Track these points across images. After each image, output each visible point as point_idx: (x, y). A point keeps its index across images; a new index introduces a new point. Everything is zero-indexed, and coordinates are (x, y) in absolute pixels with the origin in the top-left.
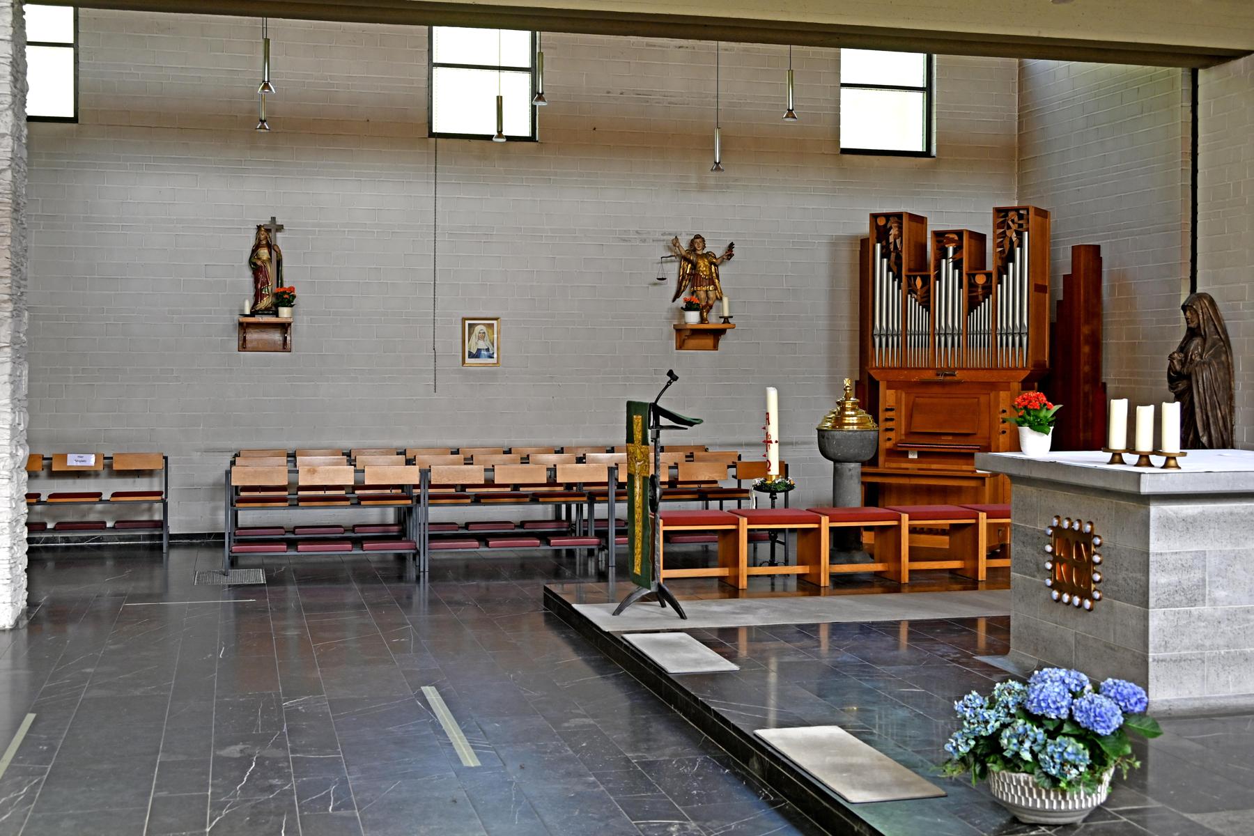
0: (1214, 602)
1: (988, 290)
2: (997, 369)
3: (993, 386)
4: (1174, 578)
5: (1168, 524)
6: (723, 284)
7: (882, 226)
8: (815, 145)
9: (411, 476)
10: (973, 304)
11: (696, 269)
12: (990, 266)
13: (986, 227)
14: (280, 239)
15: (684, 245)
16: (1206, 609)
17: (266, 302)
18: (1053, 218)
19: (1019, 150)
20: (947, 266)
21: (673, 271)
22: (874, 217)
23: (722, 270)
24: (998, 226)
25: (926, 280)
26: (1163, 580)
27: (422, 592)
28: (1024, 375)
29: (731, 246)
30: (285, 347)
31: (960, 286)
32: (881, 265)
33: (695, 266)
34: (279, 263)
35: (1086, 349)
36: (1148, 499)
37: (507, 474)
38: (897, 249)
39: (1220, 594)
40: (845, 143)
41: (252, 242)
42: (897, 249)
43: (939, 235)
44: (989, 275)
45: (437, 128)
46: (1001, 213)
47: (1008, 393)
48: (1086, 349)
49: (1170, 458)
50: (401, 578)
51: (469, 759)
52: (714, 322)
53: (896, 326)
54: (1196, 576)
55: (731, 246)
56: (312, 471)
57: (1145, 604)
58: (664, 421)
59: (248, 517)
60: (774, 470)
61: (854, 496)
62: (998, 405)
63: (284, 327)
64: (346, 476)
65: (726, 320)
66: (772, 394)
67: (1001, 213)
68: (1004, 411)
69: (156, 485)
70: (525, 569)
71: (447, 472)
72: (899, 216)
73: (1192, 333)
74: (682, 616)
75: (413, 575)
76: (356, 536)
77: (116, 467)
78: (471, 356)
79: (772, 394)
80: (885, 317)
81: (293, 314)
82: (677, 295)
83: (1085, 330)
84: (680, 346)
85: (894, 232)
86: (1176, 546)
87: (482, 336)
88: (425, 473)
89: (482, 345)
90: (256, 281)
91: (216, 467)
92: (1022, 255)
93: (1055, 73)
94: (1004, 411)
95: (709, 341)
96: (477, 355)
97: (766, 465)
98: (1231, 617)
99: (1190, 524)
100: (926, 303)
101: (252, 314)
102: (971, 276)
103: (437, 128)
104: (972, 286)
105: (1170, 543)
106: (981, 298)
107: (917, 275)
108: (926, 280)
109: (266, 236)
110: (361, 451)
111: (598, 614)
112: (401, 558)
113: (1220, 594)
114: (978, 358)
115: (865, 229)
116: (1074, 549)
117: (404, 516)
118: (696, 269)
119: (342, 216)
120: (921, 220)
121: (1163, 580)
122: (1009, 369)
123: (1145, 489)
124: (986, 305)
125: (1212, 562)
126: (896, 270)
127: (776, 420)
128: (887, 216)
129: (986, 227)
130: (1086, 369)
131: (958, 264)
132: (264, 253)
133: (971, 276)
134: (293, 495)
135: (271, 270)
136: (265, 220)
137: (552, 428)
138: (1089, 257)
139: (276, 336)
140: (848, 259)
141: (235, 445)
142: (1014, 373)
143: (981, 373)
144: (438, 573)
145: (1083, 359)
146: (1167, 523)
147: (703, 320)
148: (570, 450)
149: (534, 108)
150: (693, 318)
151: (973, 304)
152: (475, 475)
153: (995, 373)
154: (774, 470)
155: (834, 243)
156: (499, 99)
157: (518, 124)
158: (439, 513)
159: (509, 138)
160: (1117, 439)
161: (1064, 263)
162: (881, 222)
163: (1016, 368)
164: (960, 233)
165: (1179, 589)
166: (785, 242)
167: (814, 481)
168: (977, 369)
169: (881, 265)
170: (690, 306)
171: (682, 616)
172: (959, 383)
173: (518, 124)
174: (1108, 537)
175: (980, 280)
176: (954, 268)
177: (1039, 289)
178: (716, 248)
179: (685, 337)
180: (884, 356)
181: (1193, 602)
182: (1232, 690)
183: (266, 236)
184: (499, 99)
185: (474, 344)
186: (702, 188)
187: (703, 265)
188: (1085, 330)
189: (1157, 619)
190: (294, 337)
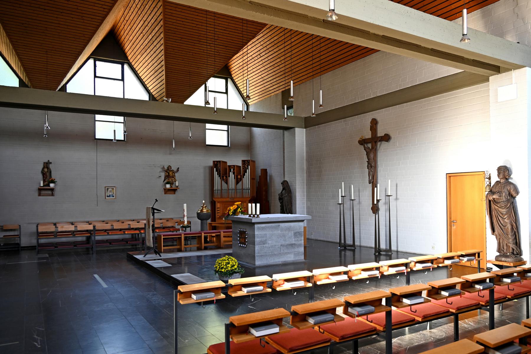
0: (269, 244)
1: (241, 179)
4: (260, 239)
5: (259, 228)
6: (176, 178)
7: (216, 164)
8: (200, 144)
9: (91, 227)
11: (169, 174)
12: (242, 174)
13: (240, 164)
14: (51, 166)
15: (166, 168)
16: (267, 245)
17: (46, 183)
18: (256, 163)
19: (249, 146)
20: (231, 174)
21: (163, 175)
22: (214, 162)
23: (176, 174)
24: (243, 164)
25: (226, 177)
26: (258, 240)
27: (95, 255)
28: (249, 199)
29: (178, 168)
30: (53, 195)
32: (215, 173)
33: (169, 173)
34: (50, 172)
35: (264, 193)
36: (254, 224)
37: (117, 226)
38: (220, 169)
39: (270, 242)
40: (207, 143)
41: (42, 167)
42: (220, 169)
43: (229, 166)
45: (97, 137)
46: (243, 161)
48: (264, 193)
49: (258, 215)
50: (88, 254)
51: (105, 286)
52: (174, 187)
53: (219, 188)
54: (265, 239)
55: (178, 168)
56: (62, 227)
57: (254, 245)
58: (155, 211)
59: (42, 241)
60: (186, 223)
61: (207, 228)
63: (52, 190)
64: (72, 228)
65: (177, 187)
66: (185, 205)
67: (243, 161)
69: (16, 233)
70: (123, 250)
71: (99, 226)
72: (220, 162)
73: (283, 189)
74: (161, 256)
75: (91, 252)
76: (75, 244)
77: (4, 228)
78: (108, 196)
79: (185, 205)
80: (217, 186)
81: (55, 185)
82: (164, 181)
83: (264, 188)
84: (165, 194)
85: (219, 165)
86: (260, 233)
87: (111, 191)
88: (94, 227)
89: (111, 194)
90: (44, 177)
91: (33, 228)
92: (248, 171)
93: (256, 130)
95: (173, 192)
96: (109, 196)
97: (184, 222)
98: (272, 247)
99: (263, 228)
100: (227, 182)
101: (44, 186)
102: (237, 176)
103: (97, 137)
105: (259, 232)
107: (224, 177)
108: (226, 177)
109: (47, 165)
110: (76, 222)
111: (140, 257)
112: (87, 249)
113: (270, 242)
115: (211, 164)
116: (242, 234)
117: (88, 238)
118: (169, 174)
119: (69, 161)
120: (226, 163)
121: (258, 240)
123: (253, 221)
124: (240, 183)
125: (268, 236)
126: (219, 174)
127: (187, 211)
128: (217, 162)
129: (240, 164)
131: (234, 173)
132: (46, 170)
133: (237, 176)
134: (55, 234)
135: (48, 174)
136: (46, 161)
137: (126, 214)
138: (265, 171)
139: (50, 192)
140: (208, 171)
141: (38, 222)
144: (98, 252)
146: (259, 228)
147: (171, 187)
148: (136, 220)
149: (124, 135)
150: (168, 186)
151: (237, 182)
152: (108, 227)
154: (186, 223)
155: (205, 168)
156: (115, 131)
157: (120, 136)
158: (98, 238)
159: (117, 140)
160: (250, 213)
161: (259, 173)
162: (216, 163)
164: (234, 166)
165: (261, 241)
166: (192, 167)
167: (196, 226)
169: (215, 173)
170: (168, 183)
171: (161, 256)
173: (120, 136)
174: (248, 231)
175: (239, 177)
177: (252, 179)
178: (174, 168)
179: (167, 191)
180: (217, 194)
181: (264, 244)
182: (272, 261)
183: (47, 165)
184: (115, 131)
185: (108, 194)
186: (170, 154)
187: (171, 173)
188: (264, 188)
189: (257, 248)
190: (56, 193)
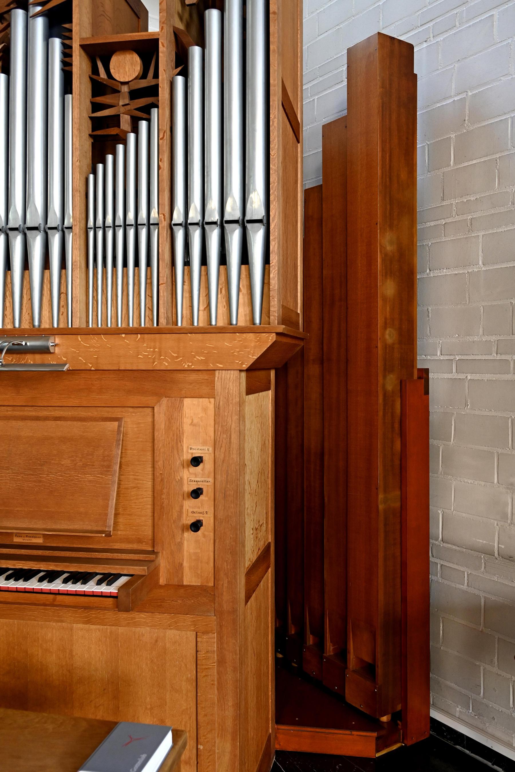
1: (146, 97)
2: (174, 330)
3: (158, 383)
10: (103, 140)
20: (220, 391)
28: (255, 347)
31: (67, 87)
44: (147, 50)
47: (209, 404)
48: (388, 288)
62: (178, 439)
68: (196, 461)
94: (196, 461)
104: (100, 88)
106: (125, 122)
114: (121, 299)
122: (209, 330)
124: (137, 147)
130: (389, 336)
142: (226, 342)
143: (128, 340)
145: (383, 311)
151: (103, 140)
153: (169, 341)
161: (324, 98)
163: (230, 329)
168: (116, 332)
172: (57, 374)
176: (49, 35)
188: (386, 242)
